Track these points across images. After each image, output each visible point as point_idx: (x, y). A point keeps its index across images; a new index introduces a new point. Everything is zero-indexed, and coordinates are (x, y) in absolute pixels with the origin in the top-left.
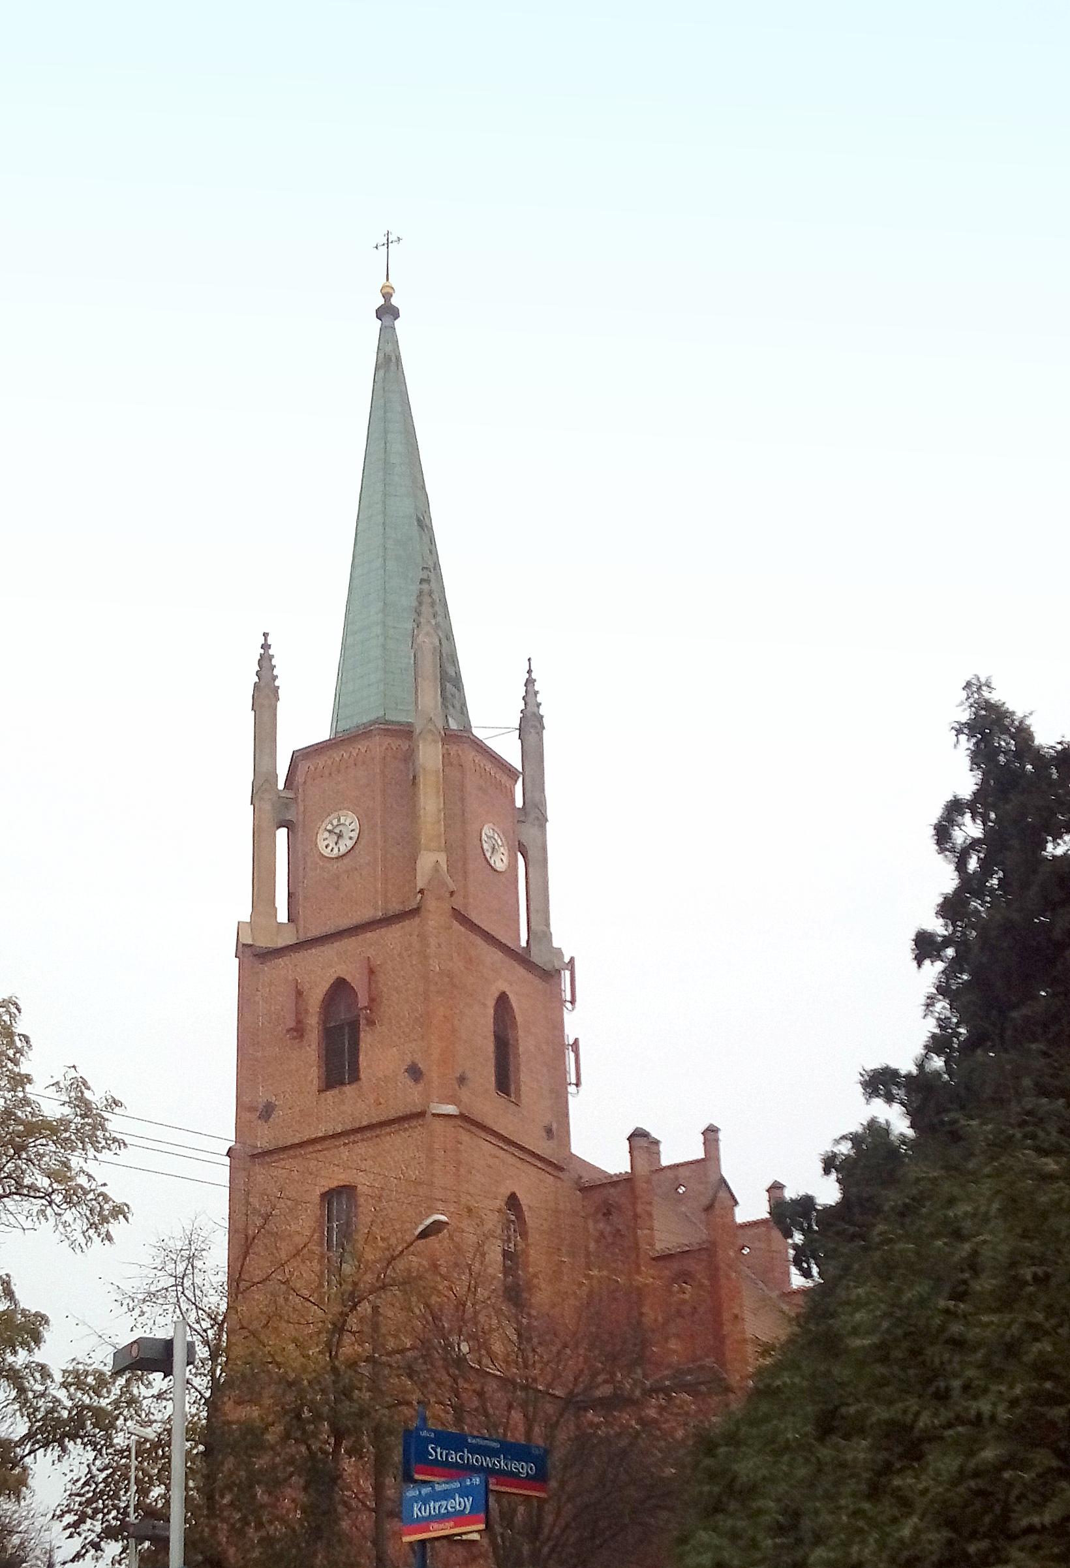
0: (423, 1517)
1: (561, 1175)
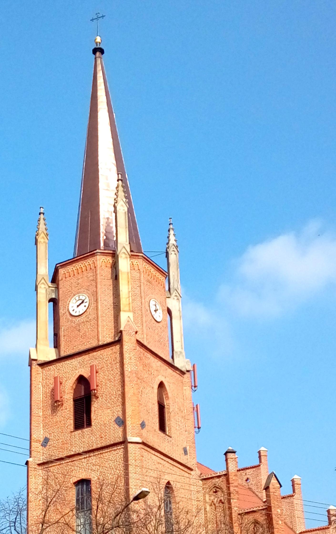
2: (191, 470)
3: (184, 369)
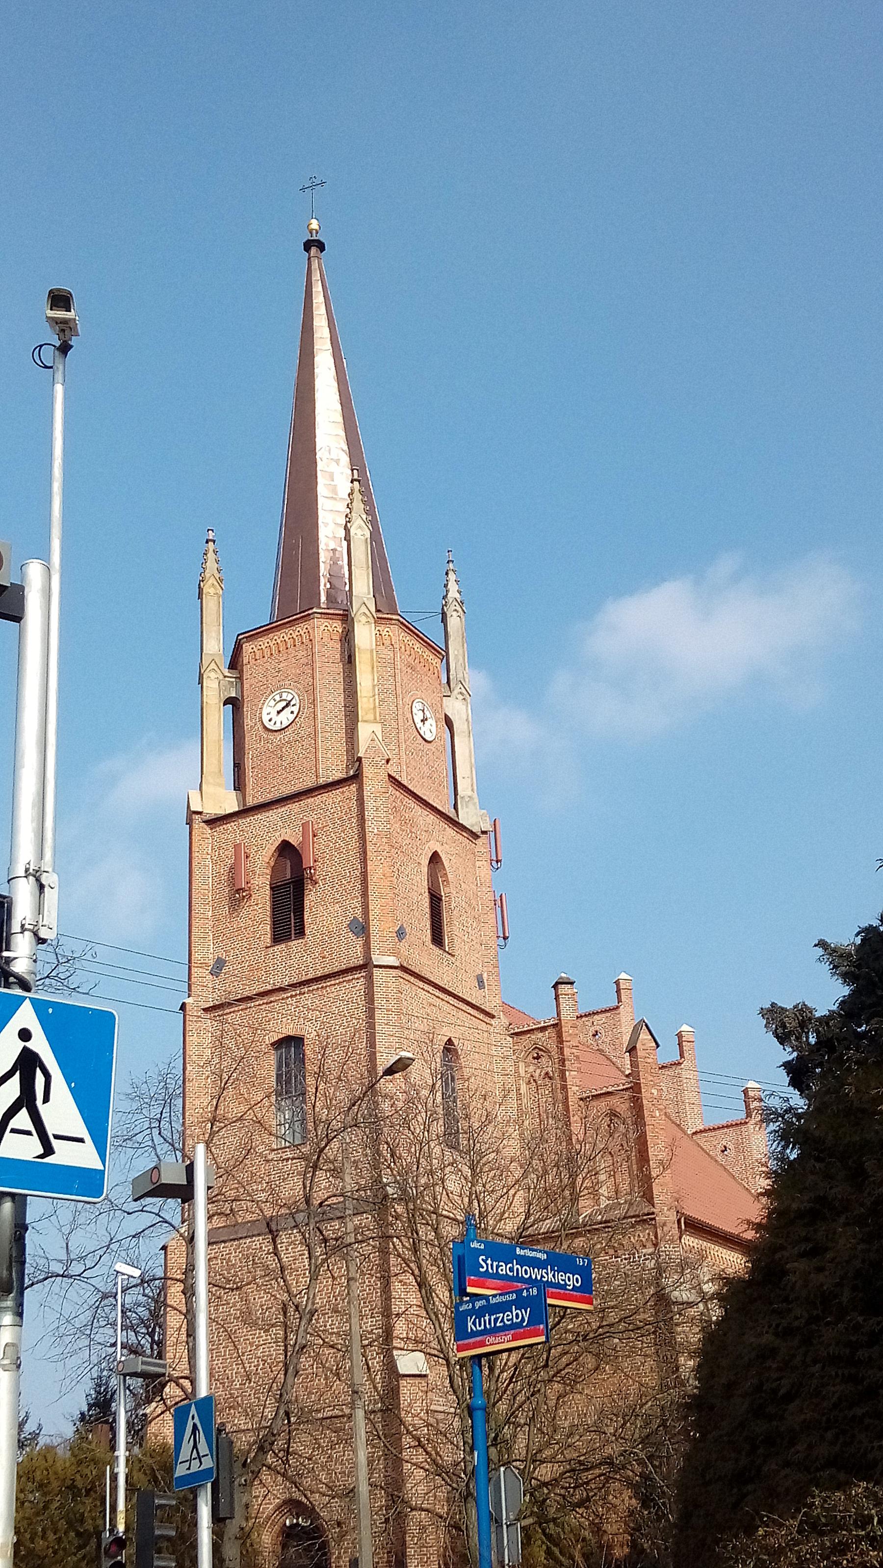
0: (477, 1331)
1: (493, 1022)
2: (493, 1017)
3: (476, 829)
